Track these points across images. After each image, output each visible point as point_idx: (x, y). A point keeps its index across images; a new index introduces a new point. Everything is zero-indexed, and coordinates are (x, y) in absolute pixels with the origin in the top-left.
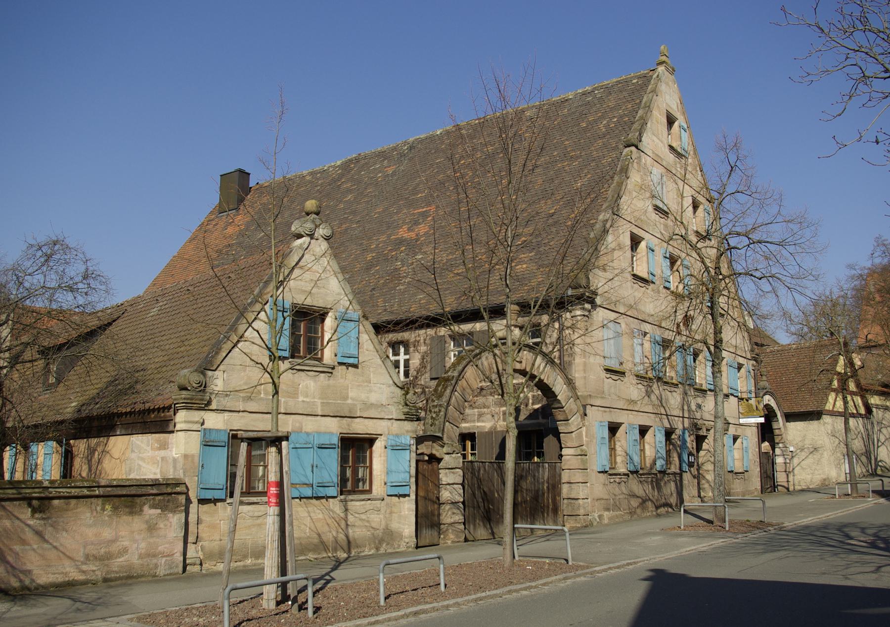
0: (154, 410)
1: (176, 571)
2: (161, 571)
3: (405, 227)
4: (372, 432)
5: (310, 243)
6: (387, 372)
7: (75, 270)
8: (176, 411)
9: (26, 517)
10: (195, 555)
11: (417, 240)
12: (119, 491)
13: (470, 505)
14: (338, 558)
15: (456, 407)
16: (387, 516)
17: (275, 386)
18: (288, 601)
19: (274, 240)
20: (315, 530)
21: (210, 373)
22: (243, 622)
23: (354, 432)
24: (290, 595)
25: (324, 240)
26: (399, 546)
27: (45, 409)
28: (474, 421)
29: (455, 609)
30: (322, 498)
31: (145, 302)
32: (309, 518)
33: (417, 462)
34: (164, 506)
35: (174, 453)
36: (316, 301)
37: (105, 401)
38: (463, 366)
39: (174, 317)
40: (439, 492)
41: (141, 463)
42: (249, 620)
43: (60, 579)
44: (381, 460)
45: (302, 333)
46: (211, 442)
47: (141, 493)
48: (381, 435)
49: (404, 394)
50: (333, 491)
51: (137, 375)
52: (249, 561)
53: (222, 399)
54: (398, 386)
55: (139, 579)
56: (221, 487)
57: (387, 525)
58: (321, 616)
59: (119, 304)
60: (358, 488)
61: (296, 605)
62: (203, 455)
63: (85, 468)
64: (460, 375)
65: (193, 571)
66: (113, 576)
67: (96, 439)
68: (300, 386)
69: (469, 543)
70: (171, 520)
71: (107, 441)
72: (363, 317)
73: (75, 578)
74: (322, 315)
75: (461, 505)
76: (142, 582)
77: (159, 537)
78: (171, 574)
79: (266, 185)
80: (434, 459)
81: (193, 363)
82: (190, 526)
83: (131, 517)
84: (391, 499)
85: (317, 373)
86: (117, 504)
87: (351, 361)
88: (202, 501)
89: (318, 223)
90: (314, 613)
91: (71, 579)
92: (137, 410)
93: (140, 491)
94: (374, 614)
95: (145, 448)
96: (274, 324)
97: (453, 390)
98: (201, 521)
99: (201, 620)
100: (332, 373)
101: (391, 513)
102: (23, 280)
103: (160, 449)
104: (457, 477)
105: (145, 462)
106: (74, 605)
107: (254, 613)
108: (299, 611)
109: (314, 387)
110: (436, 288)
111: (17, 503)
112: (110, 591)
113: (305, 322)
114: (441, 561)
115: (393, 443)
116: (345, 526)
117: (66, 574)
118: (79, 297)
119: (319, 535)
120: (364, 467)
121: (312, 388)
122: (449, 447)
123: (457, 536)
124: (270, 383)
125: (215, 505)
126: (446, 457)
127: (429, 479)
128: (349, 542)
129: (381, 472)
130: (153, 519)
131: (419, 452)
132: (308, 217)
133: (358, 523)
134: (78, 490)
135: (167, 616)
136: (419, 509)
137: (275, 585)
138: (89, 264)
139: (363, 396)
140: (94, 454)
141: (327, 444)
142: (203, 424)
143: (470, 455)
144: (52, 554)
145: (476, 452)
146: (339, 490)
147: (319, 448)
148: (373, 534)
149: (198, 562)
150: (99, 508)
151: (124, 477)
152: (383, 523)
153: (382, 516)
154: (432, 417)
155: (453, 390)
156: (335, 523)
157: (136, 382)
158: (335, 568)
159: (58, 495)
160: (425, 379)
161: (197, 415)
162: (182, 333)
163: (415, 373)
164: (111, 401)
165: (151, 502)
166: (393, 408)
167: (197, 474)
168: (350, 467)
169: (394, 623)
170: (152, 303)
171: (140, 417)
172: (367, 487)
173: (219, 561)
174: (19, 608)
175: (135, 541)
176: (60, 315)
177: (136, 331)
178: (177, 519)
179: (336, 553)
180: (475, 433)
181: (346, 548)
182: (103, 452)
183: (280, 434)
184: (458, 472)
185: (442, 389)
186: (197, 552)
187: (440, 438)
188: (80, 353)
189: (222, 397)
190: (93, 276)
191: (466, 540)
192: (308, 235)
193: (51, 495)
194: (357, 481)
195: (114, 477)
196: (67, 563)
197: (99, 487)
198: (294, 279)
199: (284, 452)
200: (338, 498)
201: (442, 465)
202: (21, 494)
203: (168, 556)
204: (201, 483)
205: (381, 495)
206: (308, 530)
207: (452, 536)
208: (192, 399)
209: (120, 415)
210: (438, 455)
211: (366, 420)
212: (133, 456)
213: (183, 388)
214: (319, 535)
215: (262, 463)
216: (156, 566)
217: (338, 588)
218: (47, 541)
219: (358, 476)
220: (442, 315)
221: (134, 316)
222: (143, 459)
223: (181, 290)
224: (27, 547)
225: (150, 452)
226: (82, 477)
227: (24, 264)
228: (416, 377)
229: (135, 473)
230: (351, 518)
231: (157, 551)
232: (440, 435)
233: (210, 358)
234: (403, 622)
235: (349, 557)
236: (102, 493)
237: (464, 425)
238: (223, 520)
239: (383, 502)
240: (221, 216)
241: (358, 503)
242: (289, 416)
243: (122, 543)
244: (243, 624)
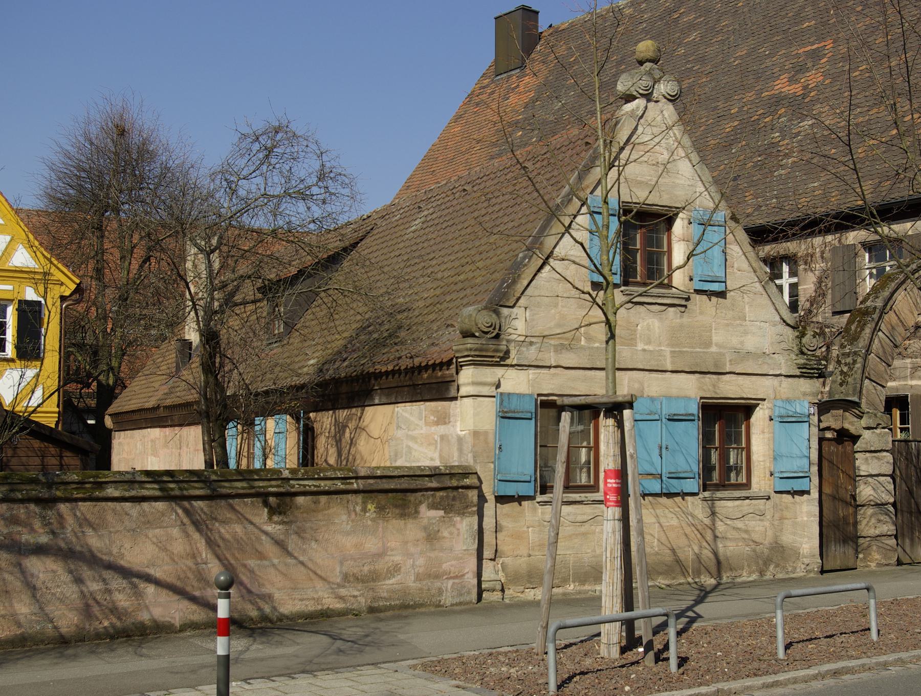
0: (427, 367)
1: (467, 598)
2: (448, 599)
3: (784, 78)
5: (646, 108)
6: (770, 303)
7: (305, 170)
8: (459, 368)
9: (262, 521)
10: (493, 577)
11: (804, 96)
12: (392, 485)
13: (905, 509)
14: (702, 586)
15: (881, 354)
16: (776, 523)
17: (610, 327)
18: (636, 647)
19: (600, 104)
20: (666, 543)
21: (505, 311)
22: (575, 675)
24: (641, 637)
25: (668, 102)
26: (795, 568)
27: (278, 369)
28: (905, 378)
29: (897, 668)
30: (676, 495)
31: (402, 211)
32: (657, 525)
33: (821, 440)
35: (458, 429)
36: (660, 199)
37: (355, 356)
38: (890, 290)
39: (446, 231)
40: (855, 488)
41: (411, 444)
42: (582, 673)
43: (311, 607)
44: (764, 438)
45: (638, 247)
46: (512, 412)
47: (415, 487)
48: (764, 400)
49: (797, 337)
50: (692, 485)
51: (399, 317)
52: (571, 587)
54: (788, 325)
55: (417, 610)
56: (528, 479)
57: (776, 537)
58: (689, 672)
59: (365, 217)
60: (729, 480)
61: (651, 654)
62: (500, 432)
63: (333, 451)
64: (885, 305)
65: (492, 599)
66: (381, 604)
67: (346, 410)
68: (639, 327)
69: (904, 566)
70: (458, 526)
71: (362, 414)
72: (732, 218)
73: (331, 607)
74: (666, 218)
75: (892, 509)
76: (422, 613)
77: (442, 550)
78: (460, 604)
79: (563, 27)
80: (845, 437)
81: (479, 298)
83: (403, 521)
84: (781, 498)
85: (664, 308)
86: (383, 503)
87: (715, 287)
88: (502, 499)
89: (657, 77)
90: (680, 666)
91: (325, 607)
92: (402, 368)
93: (414, 484)
94: (770, 671)
95: (416, 422)
96: (605, 233)
97: (876, 329)
98: (501, 527)
99: (512, 670)
100: (685, 306)
101: (782, 518)
102: (236, 186)
103: (437, 423)
104: (884, 464)
105: (416, 442)
106: (333, 644)
107: (588, 663)
108: (656, 662)
110: (852, 167)
111: (248, 500)
112: (380, 625)
113: (644, 230)
114: (871, 594)
115: (783, 412)
116: (712, 537)
117: (318, 600)
118: (314, 208)
119: (673, 551)
120: (738, 449)
121: (657, 331)
122: (870, 417)
123: (885, 557)
124: (602, 322)
125: (521, 505)
126: (867, 434)
127: (839, 468)
128: (719, 563)
129: (764, 455)
130: (433, 524)
131: (823, 425)
132: (642, 68)
133: (731, 534)
134: (329, 483)
135: (464, 663)
136: (824, 514)
137: (618, 624)
138: (325, 158)
139: (735, 341)
140: (344, 432)
141: (680, 415)
142: (498, 386)
143: (899, 430)
144: (299, 573)
145: (910, 426)
146: (701, 483)
147: (669, 420)
148: (754, 551)
149: (499, 587)
150: (358, 508)
151: (388, 464)
152: (770, 533)
153: (767, 524)
154: (842, 372)
155: (875, 329)
156: (696, 532)
157: (400, 327)
158: (700, 600)
159: (302, 489)
160: (823, 314)
161: (491, 374)
162: (460, 255)
163: (808, 305)
164: (364, 356)
165: (430, 500)
166: (781, 357)
167: (493, 460)
168: (716, 449)
169: (803, 686)
170: (413, 212)
171: (407, 377)
172: (743, 479)
174: (260, 647)
175: (409, 555)
176: (289, 235)
177: (392, 255)
178: (467, 525)
179: (699, 577)
180: (907, 396)
181: (713, 569)
182: (356, 429)
183: (620, 399)
184: (885, 456)
185: (857, 327)
186: (497, 572)
187: (857, 405)
188: (319, 287)
190: (332, 175)
191: (899, 563)
192: (642, 95)
193: (293, 490)
194: (727, 469)
195: (374, 464)
196: (319, 584)
197: (357, 478)
198: (635, 161)
199: (627, 425)
200: (701, 496)
201: (859, 445)
202: (254, 488)
203: (456, 577)
204: (499, 473)
205: (765, 491)
206: (656, 543)
207: (877, 556)
208: (481, 350)
209: (378, 375)
210: (853, 430)
211: (741, 378)
212: (399, 434)
213: (467, 334)
214: (673, 551)
215: (585, 444)
216: (440, 592)
217: (709, 630)
218: (290, 554)
219: (728, 462)
220: (861, 209)
221: (387, 232)
222: (413, 439)
223: (454, 191)
224: (266, 563)
225: (424, 428)
226: (328, 464)
227: (236, 163)
228: (810, 311)
229: (404, 458)
230: (720, 527)
232: (856, 399)
233: (505, 288)
234: (817, 685)
235: (719, 584)
236: (361, 487)
237: (890, 384)
239: (768, 502)
240: (498, 80)
241: (730, 504)
243: (392, 558)
244: (575, 679)
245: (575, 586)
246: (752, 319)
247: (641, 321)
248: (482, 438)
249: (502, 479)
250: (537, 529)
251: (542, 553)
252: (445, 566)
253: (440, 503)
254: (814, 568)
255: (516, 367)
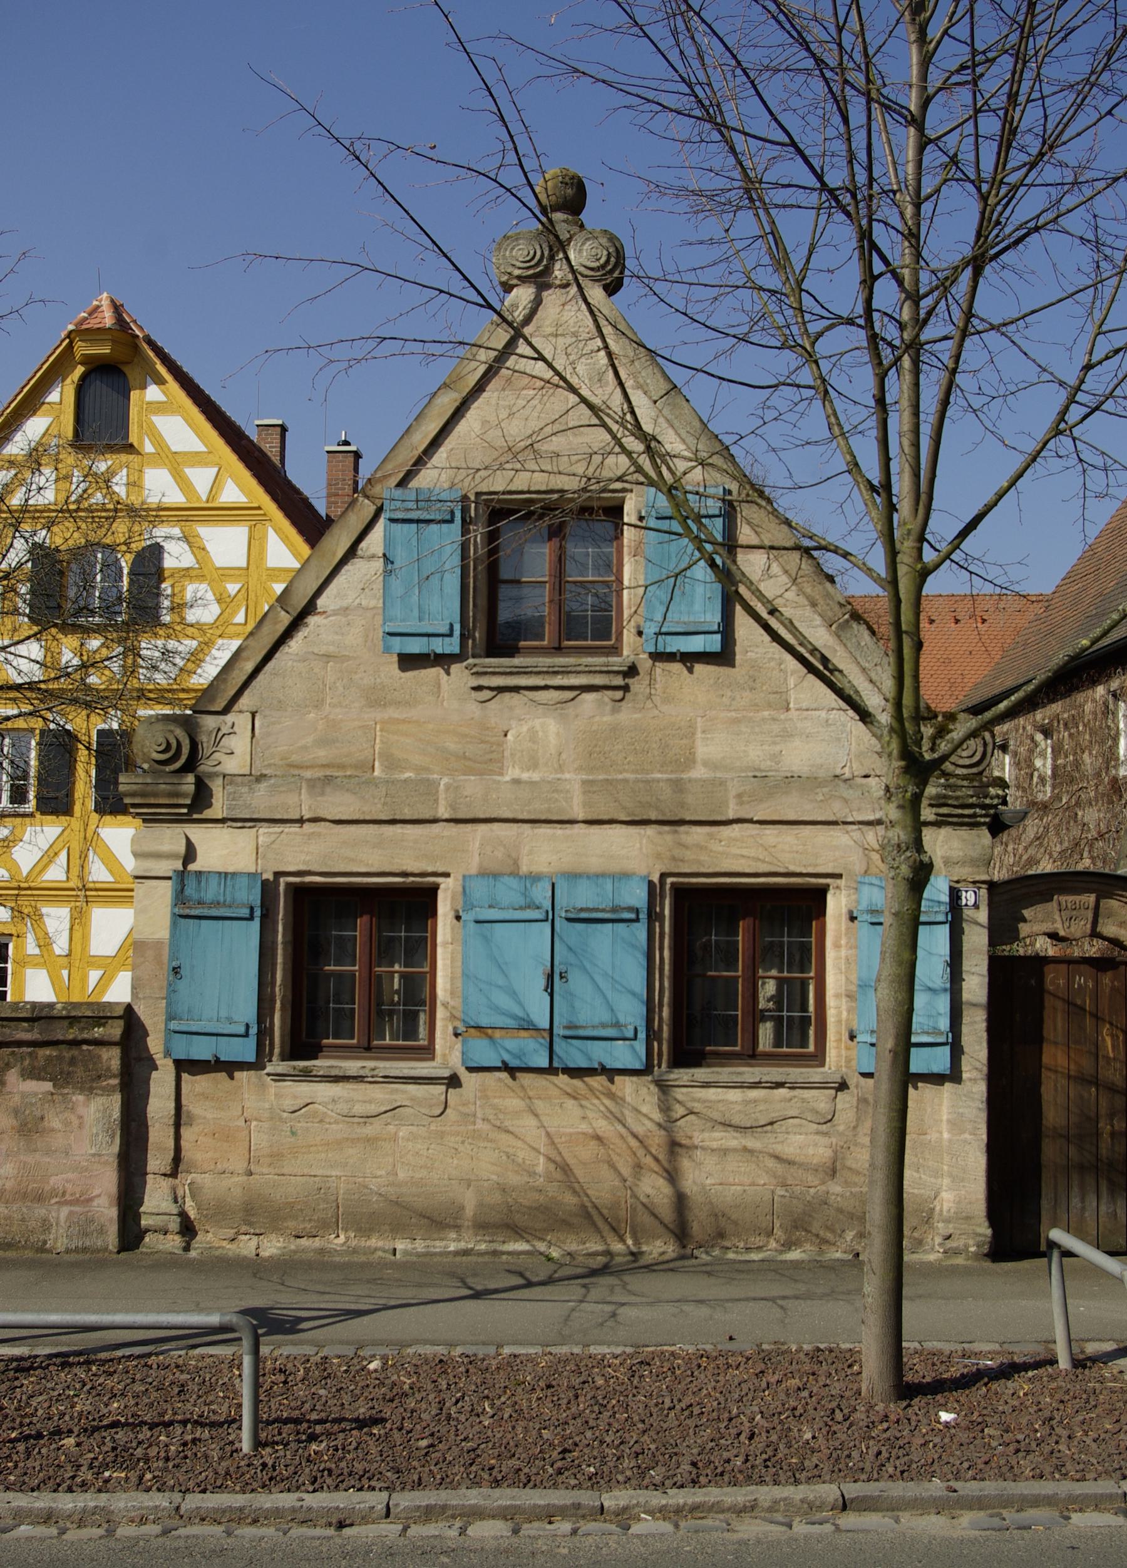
2: (59, 1240)
4: (793, 868)
23: (717, 870)
34: (61, 1073)
52: (339, 1241)
53: (245, 789)
65: (161, 1247)
70: (81, 1110)
77: (48, 1152)
78: (85, 1250)
82: (151, 1129)
85: (570, 694)
88: (184, 1066)
109: (558, 734)
125: (232, 1078)
130: (32, 1104)
139: (756, 753)
147: (569, 920)
165: (27, 1062)
173: (244, 1229)
189: (243, 784)
208: (143, 795)
211: (770, 831)
231: (47, 1188)
238: (256, 1120)
242: (469, 827)
245: (348, 1239)
246: (804, 705)
247: (514, 723)
248: (150, 954)
249: (177, 1029)
250: (266, 1125)
251: (277, 1171)
252: (55, 1181)
253: (44, 1068)
254: (967, 1246)
255: (230, 823)
